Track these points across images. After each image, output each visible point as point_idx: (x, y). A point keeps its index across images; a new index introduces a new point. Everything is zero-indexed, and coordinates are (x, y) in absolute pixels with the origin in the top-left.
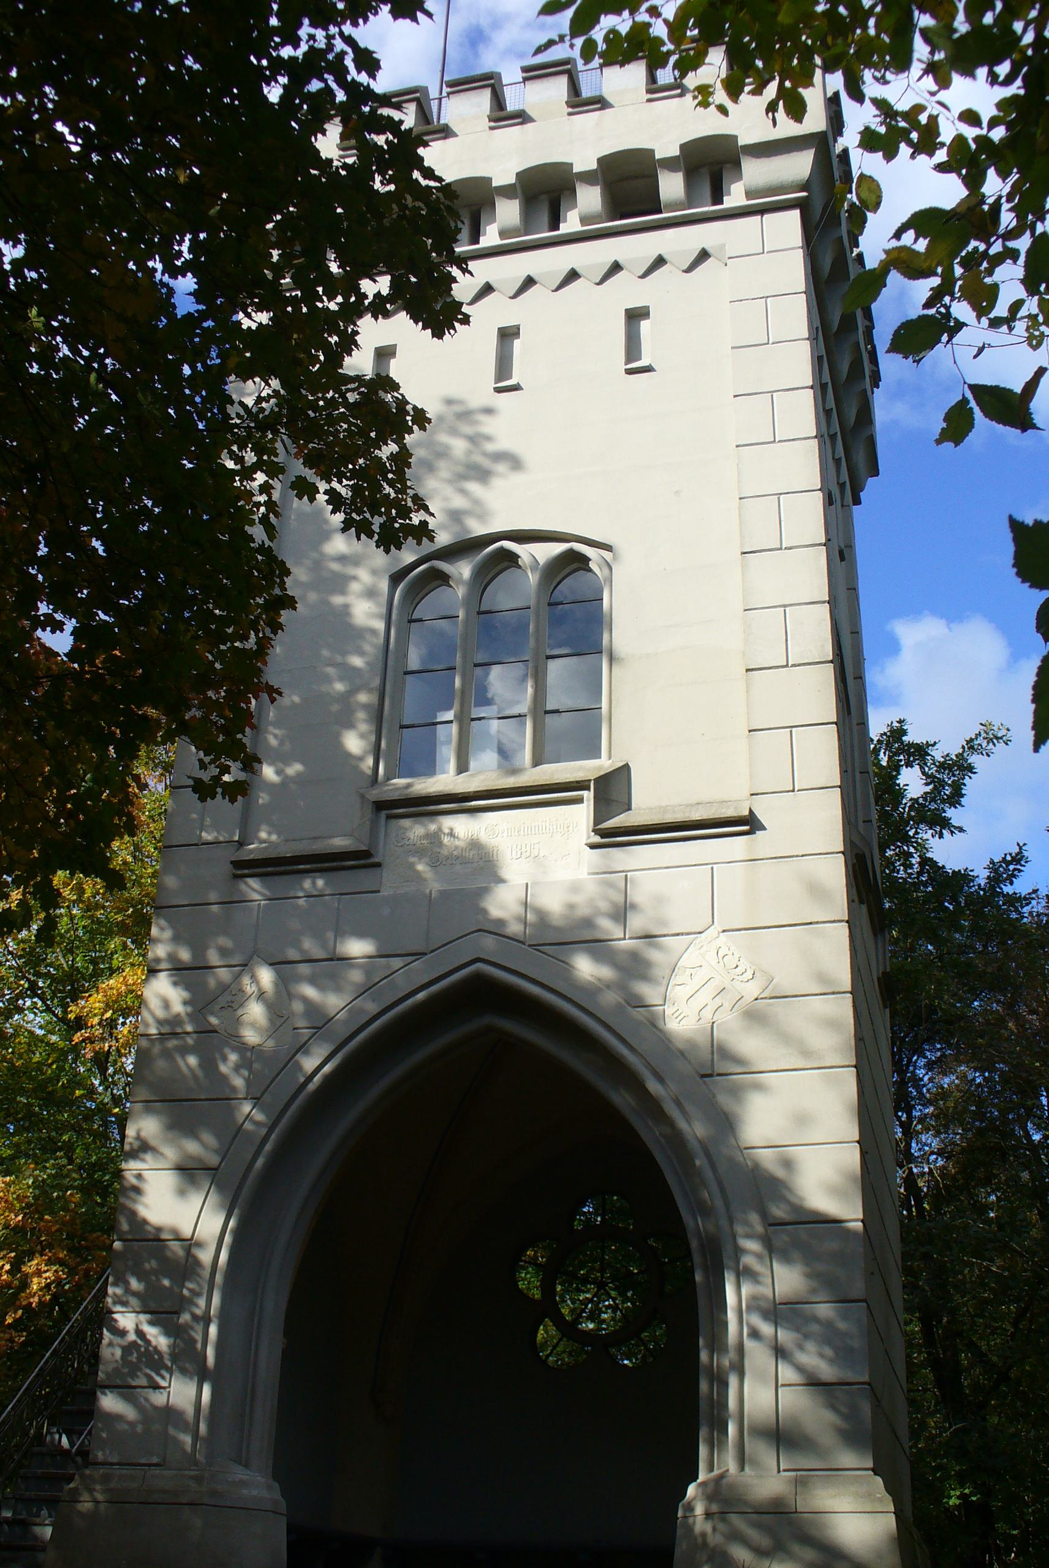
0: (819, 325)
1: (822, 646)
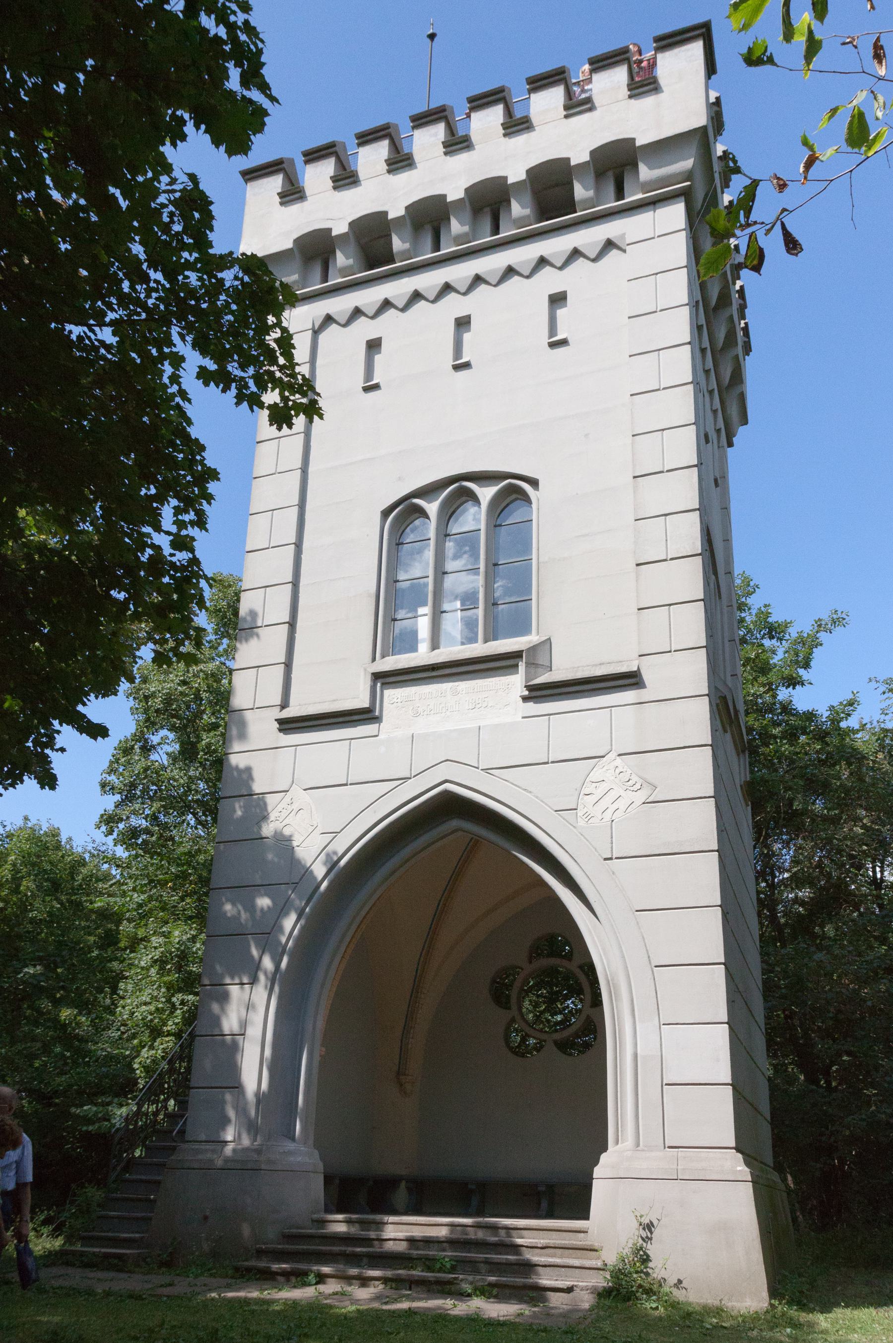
0: (700, 298)
1: (693, 543)
